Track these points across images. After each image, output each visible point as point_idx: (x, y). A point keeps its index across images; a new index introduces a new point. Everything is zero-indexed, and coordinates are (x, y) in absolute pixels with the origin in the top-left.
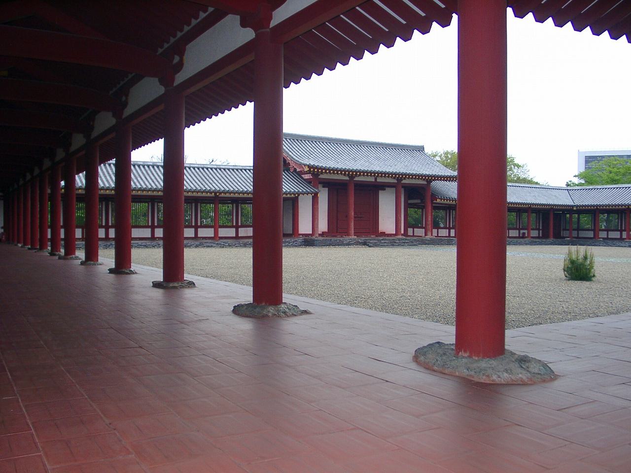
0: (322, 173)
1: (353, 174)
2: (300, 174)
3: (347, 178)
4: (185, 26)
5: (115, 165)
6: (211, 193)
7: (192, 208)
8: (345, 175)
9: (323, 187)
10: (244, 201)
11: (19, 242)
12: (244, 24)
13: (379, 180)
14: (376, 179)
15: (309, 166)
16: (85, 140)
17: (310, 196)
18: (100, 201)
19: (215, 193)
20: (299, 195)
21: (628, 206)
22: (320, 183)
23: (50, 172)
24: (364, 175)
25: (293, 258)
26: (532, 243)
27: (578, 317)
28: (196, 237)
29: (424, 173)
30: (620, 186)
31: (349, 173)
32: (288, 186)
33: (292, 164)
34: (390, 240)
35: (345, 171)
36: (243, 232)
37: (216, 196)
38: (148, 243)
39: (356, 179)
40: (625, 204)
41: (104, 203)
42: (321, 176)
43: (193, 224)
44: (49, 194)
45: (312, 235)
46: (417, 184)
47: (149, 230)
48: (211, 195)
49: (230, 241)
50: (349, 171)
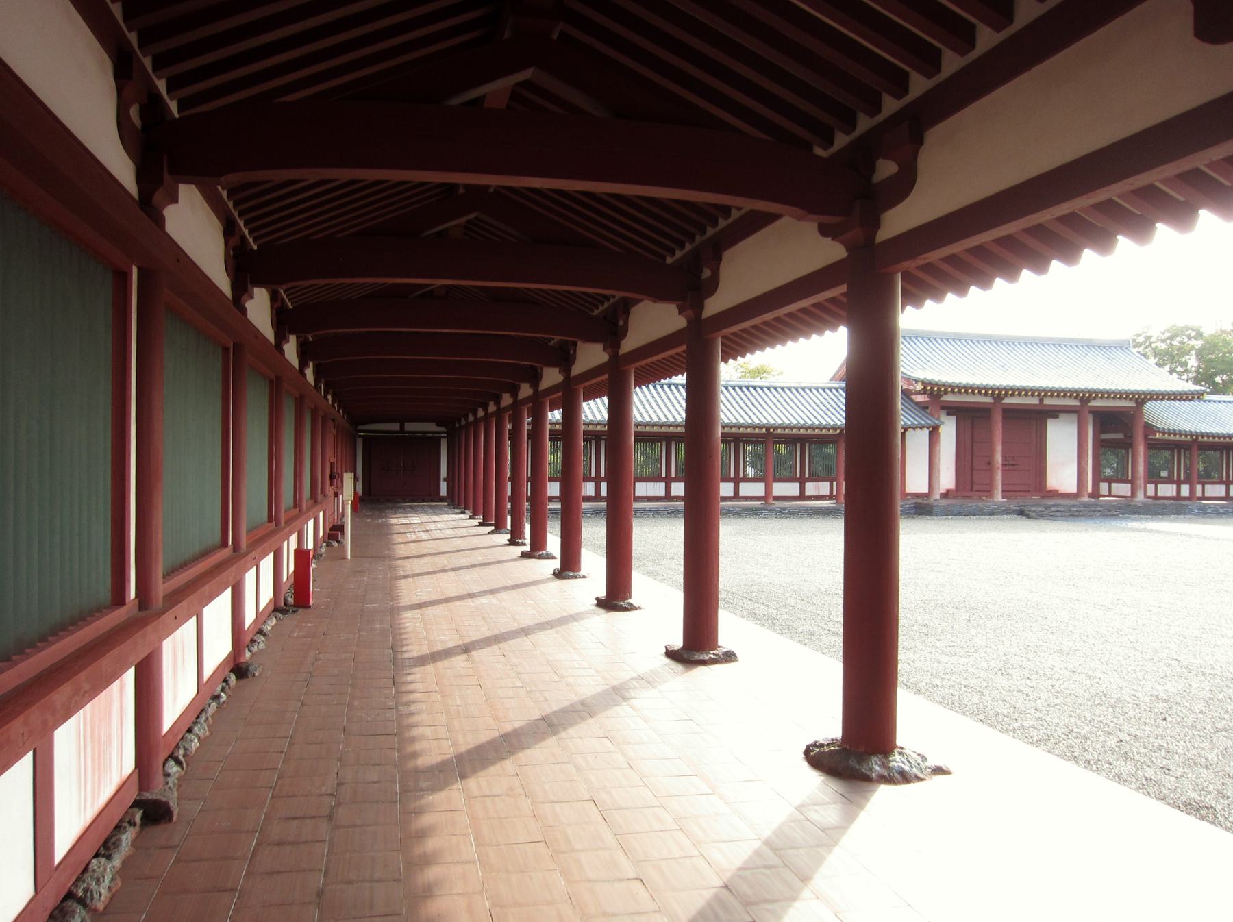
0: (946, 392)
3: (989, 400)
6: (761, 428)
9: (948, 414)
13: (1047, 402)
14: (1041, 401)
17: (926, 432)
19: (768, 429)
22: (943, 408)
39: (1007, 401)
42: (945, 398)
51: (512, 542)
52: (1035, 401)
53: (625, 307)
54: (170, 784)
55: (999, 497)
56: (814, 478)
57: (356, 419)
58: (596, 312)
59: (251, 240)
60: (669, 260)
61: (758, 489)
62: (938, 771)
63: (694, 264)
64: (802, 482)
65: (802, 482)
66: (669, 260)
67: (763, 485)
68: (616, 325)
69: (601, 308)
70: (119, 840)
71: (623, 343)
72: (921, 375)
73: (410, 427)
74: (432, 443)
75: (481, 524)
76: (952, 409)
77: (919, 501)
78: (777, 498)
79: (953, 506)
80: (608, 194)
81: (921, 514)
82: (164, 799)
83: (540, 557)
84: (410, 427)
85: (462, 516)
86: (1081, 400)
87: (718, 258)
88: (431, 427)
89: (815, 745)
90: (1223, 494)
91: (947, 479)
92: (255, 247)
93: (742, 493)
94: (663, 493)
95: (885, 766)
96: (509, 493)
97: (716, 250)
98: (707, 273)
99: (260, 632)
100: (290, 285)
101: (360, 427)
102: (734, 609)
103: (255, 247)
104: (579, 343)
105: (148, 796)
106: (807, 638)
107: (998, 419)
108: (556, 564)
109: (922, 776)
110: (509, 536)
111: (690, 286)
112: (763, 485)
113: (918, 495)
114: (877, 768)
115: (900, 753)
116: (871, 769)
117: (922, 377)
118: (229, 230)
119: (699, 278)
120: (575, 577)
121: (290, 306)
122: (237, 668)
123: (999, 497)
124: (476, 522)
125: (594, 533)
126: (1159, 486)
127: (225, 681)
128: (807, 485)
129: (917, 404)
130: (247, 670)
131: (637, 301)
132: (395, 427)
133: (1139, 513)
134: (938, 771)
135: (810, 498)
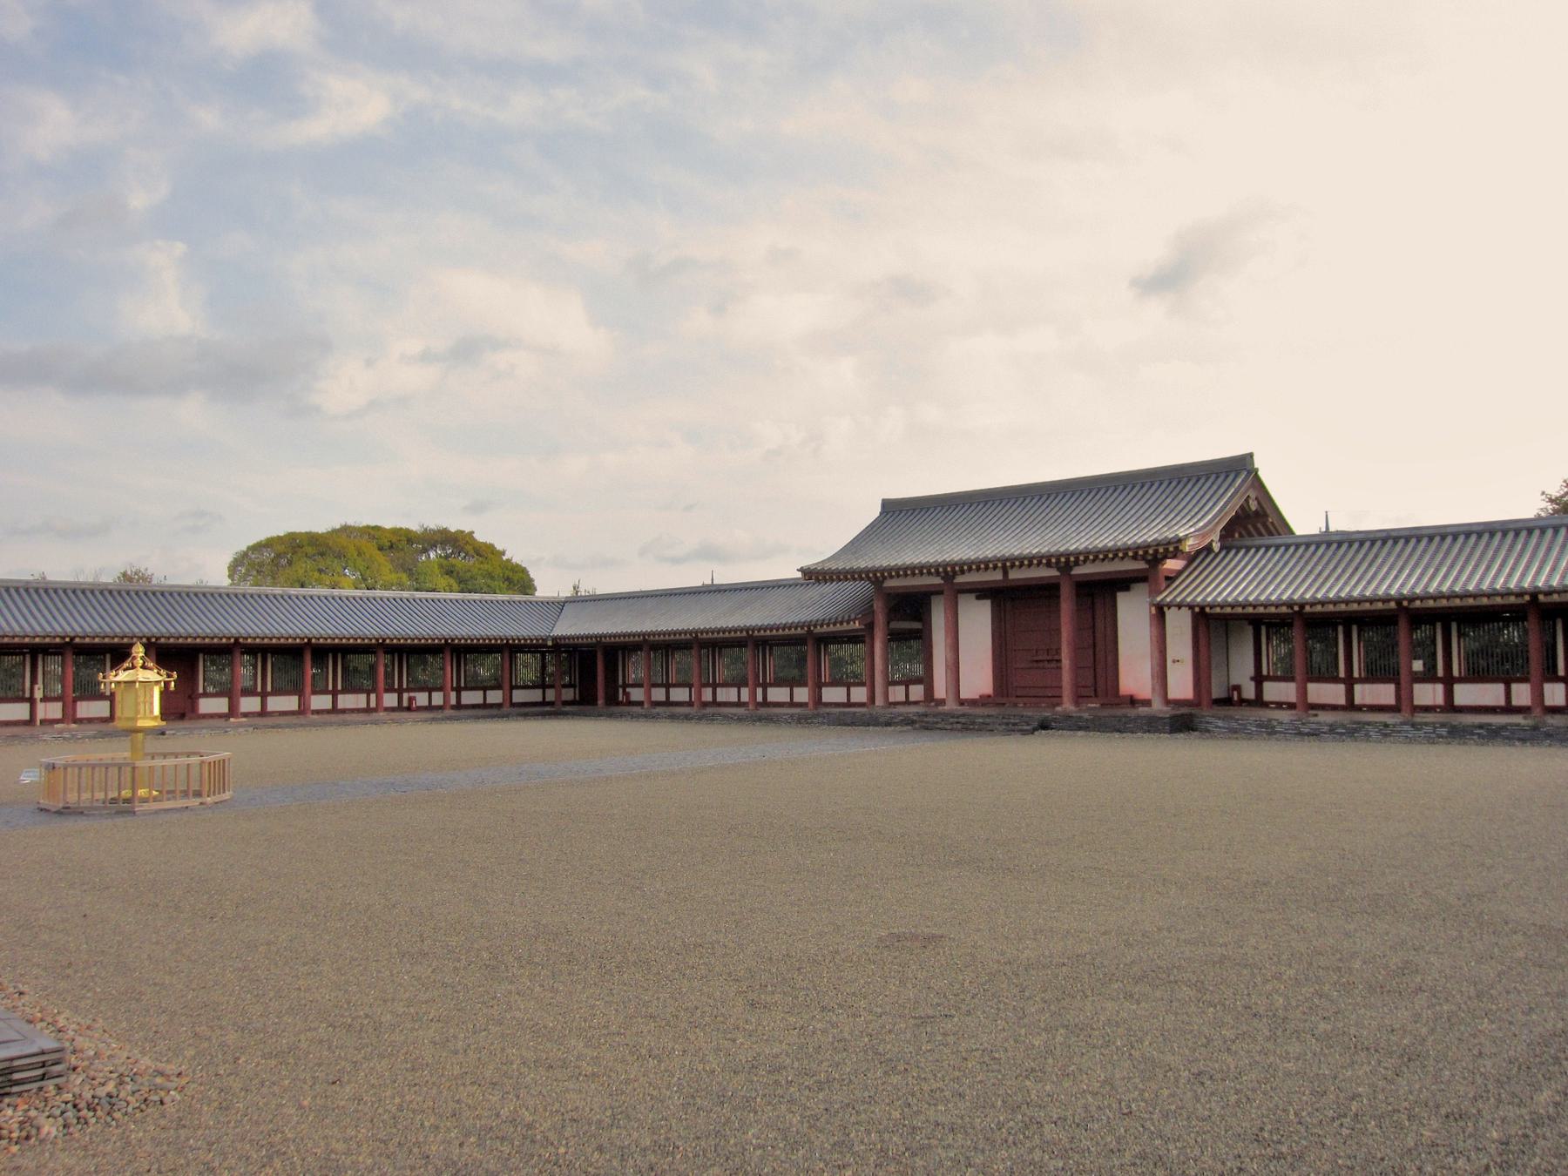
0: (1077, 563)
1: (1068, 560)
3: (1054, 573)
7: (872, 653)
8: (1135, 557)
13: (1014, 575)
14: (1005, 573)
21: (1302, 606)
24: (921, 574)
26: (1431, 741)
28: (263, 713)
29: (899, 562)
30: (477, 596)
31: (1146, 552)
34: (968, 720)
35: (1049, 557)
37: (645, 641)
38: (294, 720)
39: (1077, 571)
40: (1225, 600)
41: (1439, 626)
43: (1342, 674)
46: (1126, 572)
48: (1519, 601)
49: (355, 717)
50: (1058, 556)
52: (997, 576)
55: (1068, 706)
56: (277, 692)
64: (264, 695)
65: (264, 695)
67: (226, 700)
76: (982, 592)
86: (1058, 565)
90: (1440, 700)
91: (1181, 684)
93: (270, 708)
94: (1342, 701)
107: (1066, 592)
112: (226, 700)
123: (1068, 706)
126: (853, 689)
128: (1457, 688)
133: (1086, 729)
135: (1359, 708)
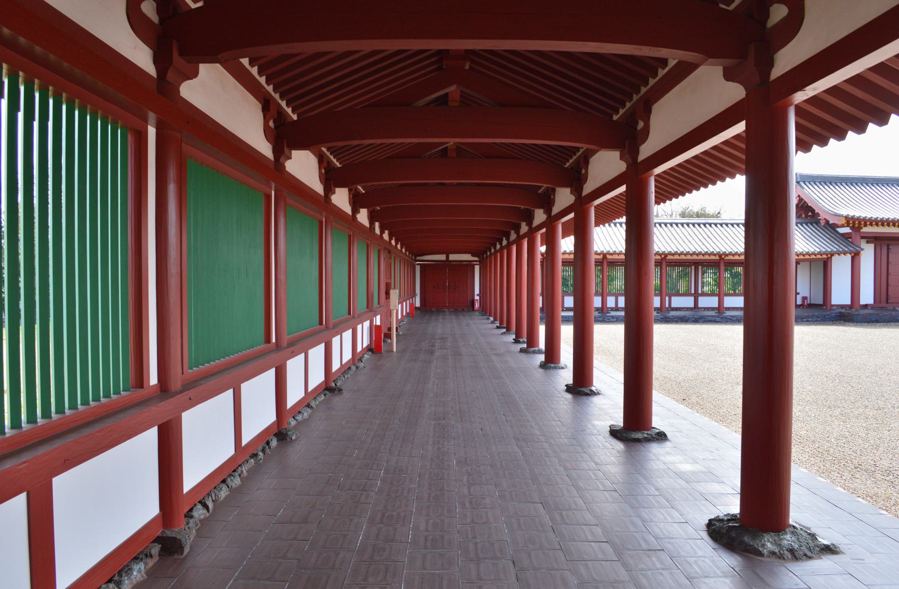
2: (833, 227)
4: (651, 79)
5: (627, 223)
6: (715, 255)
9: (868, 242)
10: (613, 264)
11: (490, 315)
12: (729, 75)
15: (846, 217)
16: (573, 198)
17: (849, 257)
18: (656, 266)
19: (720, 256)
20: (832, 255)
22: (862, 238)
23: (544, 230)
25: (808, 342)
27: (598, 531)
32: (802, 241)
33: (823, 216)
36: (729, 302)
42: (865, 230)
43: (693, 292)
44: (542, 254)
45: (851, 306)
47: (716, 298)
51: (516, 341)
53: (585, 160)
54: (191, 525)
57: (416, 252)
58: (568, 164)
59: (289, 110)
60: (615, 118)
61: (713, 302)
62: (829, 550)
63: (631, 119)
66: (615, 118)
68: (580, 173)
69: (571, 161)
70: (131, 569)
71: (585, 186)
72: (844, 212)
73: (452, 257)
74: (470, 266)
75: (498, 327)
76: (870, 238)
77: (843, 311)
78: (728, 309)
79: (870, 314)
80: (531, 52)
81: (840, 320)
82: (179, 537)
83: (534, 352)
84: (452, 257)
85: (487, 321)
87: (648, 112)
88: (467, 257)
89: (718, 519)
91: (867, 296)
92: (295, 117)
95: (775, 543)
96: (541, 305)
97: (645, 108)
98: (641, 124)
99: (308, 406)
100: (331, 145)
101: (418, 258)
102: (668, 393)
103: (295, 117)
104: (557, 189)
105: (169, 533)
106: (723, 420)
108: (542, 358)
109: (809, 554)
110: (514, 337)
111: (627, 138)
113: (842, 306)
114: (769, 545)
115: (792, 533)
116: (763, 545)
117: (845, 213)
118: (267, 105)
119: (636, 129)
120: (555, 368)
121: (338, 164)
122: (279, 432)
124: (494, 326)
125: (609, 339)
127: (268, 443)
129: (843, 235)
130: (286, 434)
131: (594, 152)
132: (442, 257)
134: (829, 550)
